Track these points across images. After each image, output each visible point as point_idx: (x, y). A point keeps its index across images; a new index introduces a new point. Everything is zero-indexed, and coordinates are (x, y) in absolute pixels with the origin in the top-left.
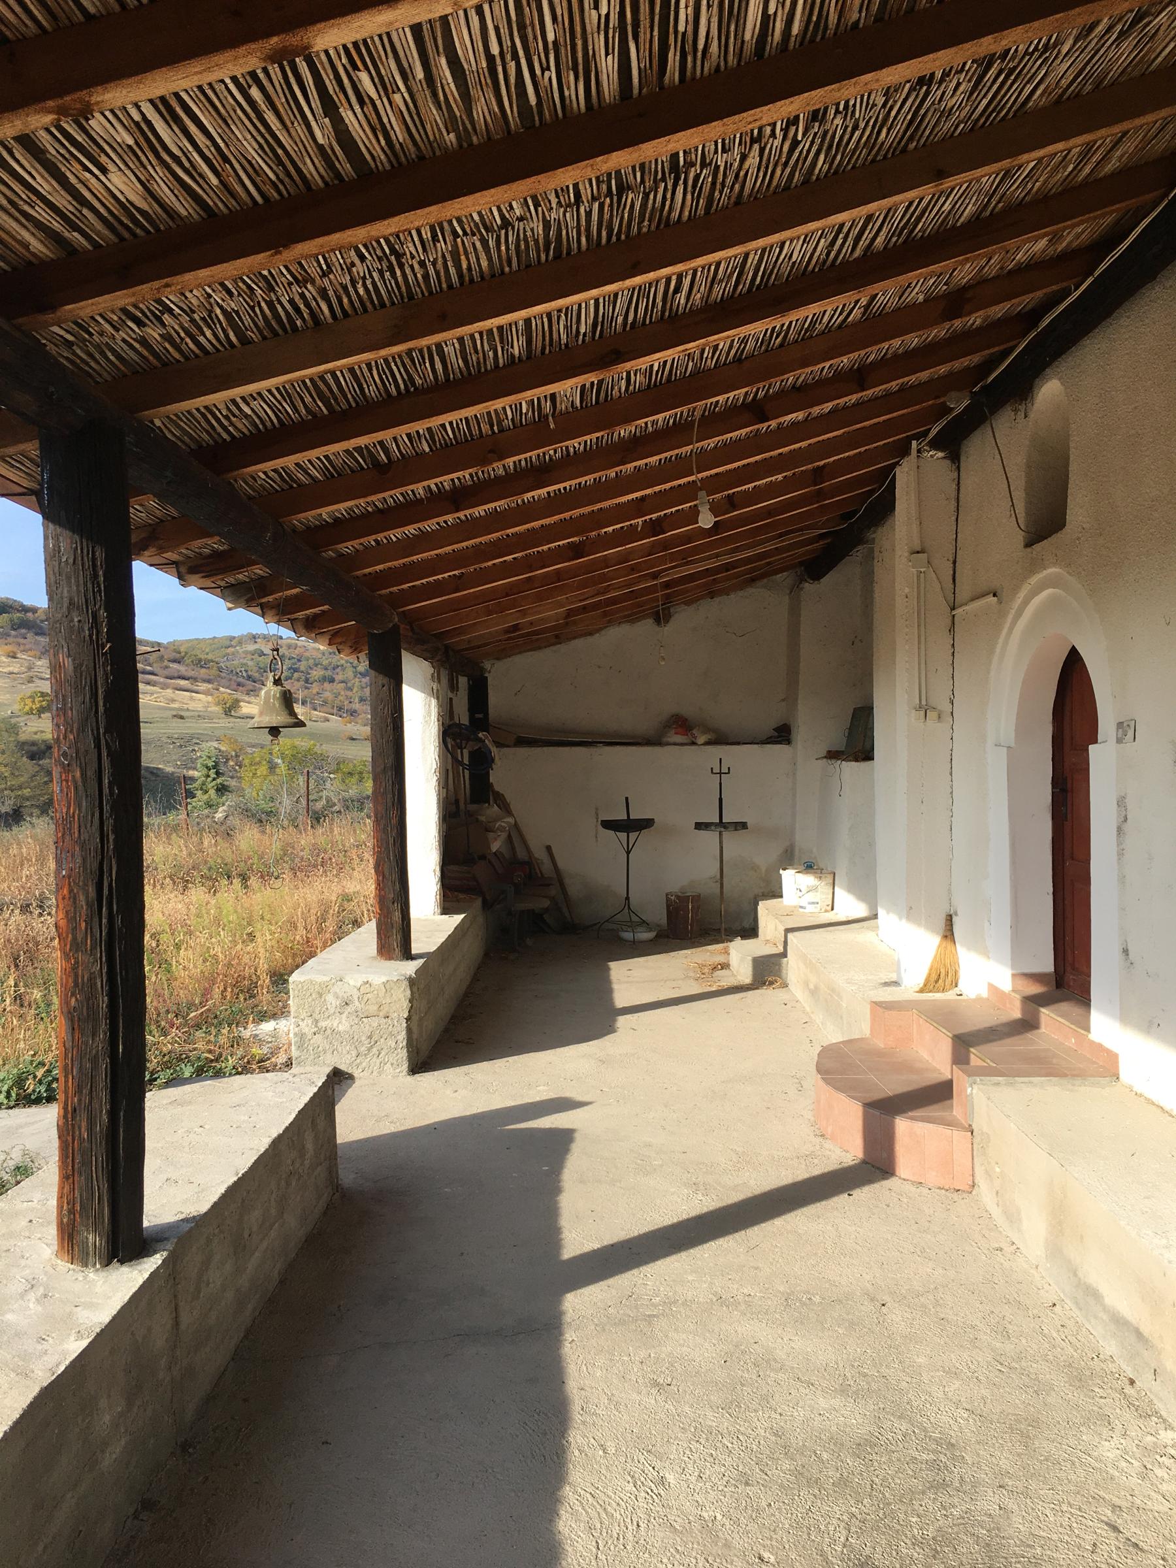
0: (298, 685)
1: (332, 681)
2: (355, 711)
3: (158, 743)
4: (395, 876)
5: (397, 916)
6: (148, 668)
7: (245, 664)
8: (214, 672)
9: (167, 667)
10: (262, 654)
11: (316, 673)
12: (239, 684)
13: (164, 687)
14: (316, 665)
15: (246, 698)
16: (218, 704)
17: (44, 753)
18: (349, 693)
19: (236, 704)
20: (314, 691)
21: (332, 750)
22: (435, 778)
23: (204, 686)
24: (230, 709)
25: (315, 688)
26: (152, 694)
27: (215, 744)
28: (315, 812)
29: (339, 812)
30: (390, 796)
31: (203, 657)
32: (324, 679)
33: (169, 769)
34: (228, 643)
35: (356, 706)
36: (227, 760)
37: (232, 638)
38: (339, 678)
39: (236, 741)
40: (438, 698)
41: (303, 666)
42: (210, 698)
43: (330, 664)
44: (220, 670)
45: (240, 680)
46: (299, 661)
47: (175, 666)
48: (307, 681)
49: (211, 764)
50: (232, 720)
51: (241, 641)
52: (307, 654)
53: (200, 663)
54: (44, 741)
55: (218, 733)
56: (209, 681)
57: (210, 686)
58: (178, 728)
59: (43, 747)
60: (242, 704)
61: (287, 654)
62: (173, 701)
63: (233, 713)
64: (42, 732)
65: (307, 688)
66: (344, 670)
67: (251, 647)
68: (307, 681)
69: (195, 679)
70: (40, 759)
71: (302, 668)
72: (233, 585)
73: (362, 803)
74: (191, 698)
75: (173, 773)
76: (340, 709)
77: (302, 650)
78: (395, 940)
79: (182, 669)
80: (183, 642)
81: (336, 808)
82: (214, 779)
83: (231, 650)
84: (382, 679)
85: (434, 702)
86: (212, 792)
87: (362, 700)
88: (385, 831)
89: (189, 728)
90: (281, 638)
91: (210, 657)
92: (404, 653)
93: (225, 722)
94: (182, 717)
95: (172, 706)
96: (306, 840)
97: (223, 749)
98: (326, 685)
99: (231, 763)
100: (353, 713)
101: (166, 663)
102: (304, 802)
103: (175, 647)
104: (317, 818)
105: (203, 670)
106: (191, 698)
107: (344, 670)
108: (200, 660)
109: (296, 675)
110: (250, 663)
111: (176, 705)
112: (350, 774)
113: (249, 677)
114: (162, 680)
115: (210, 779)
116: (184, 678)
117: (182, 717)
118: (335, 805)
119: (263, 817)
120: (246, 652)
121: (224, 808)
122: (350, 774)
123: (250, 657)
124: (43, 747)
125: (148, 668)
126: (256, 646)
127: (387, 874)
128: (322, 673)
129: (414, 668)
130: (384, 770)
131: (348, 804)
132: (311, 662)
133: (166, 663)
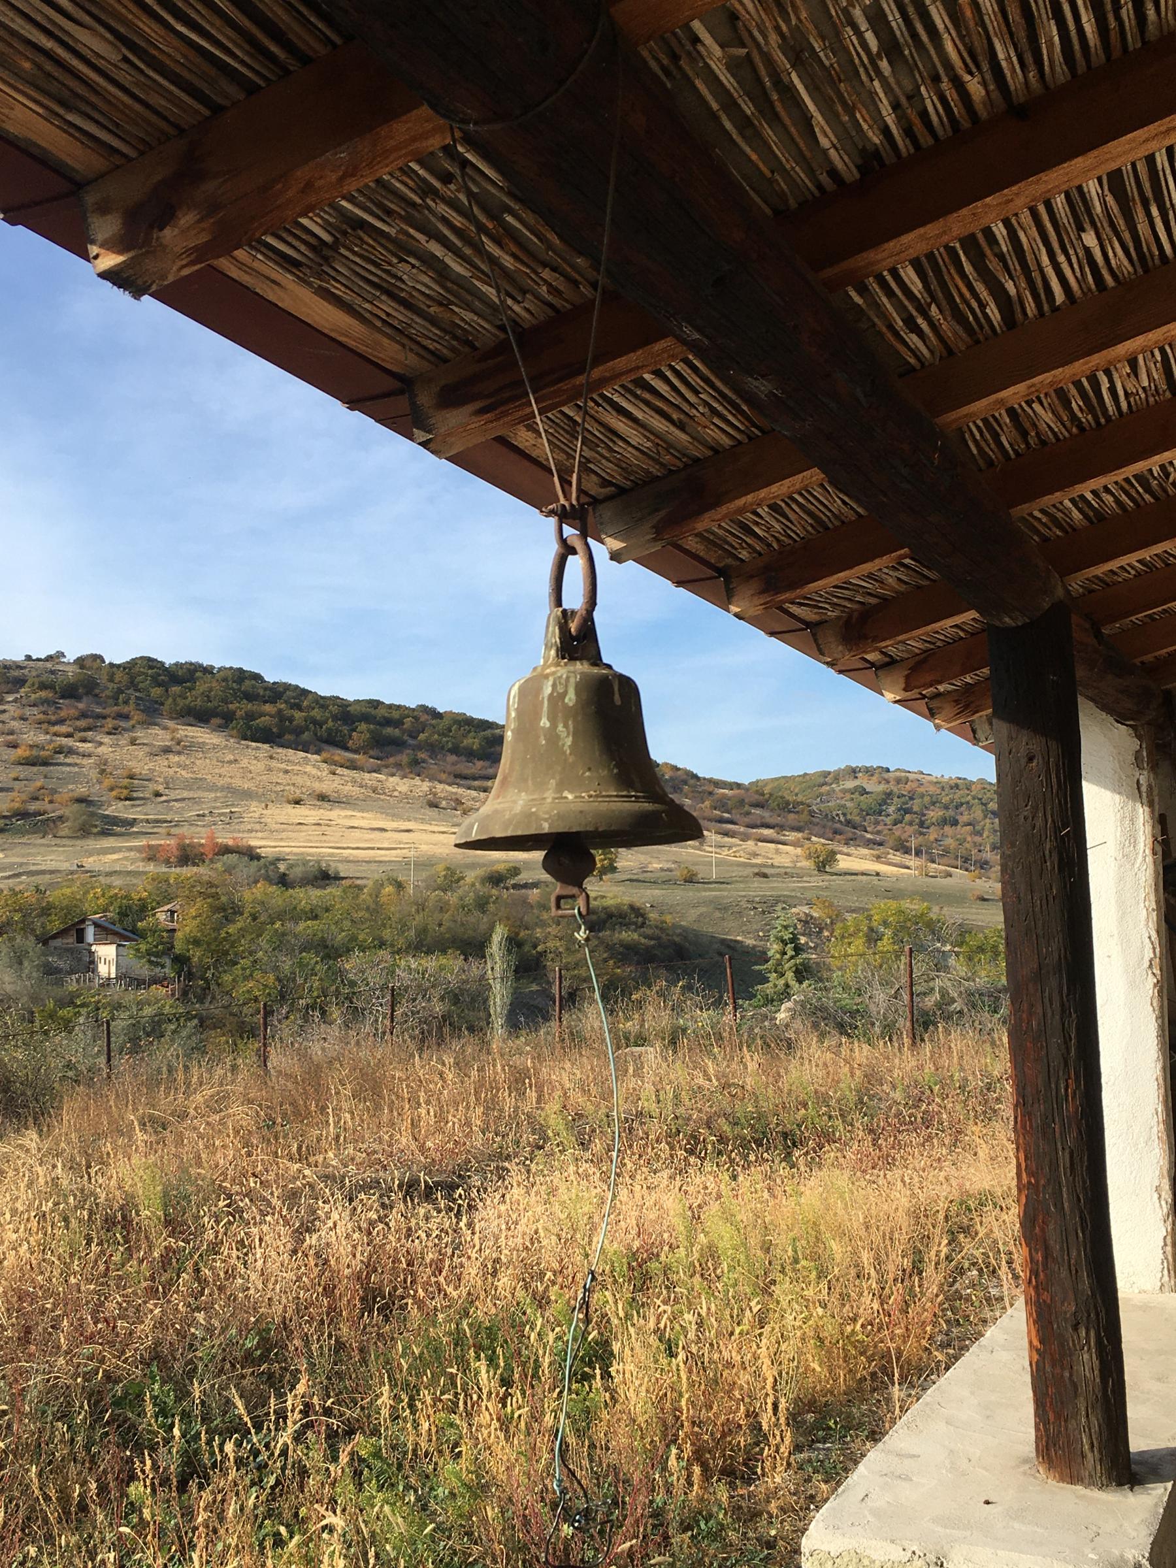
0: (910, 830)
1: (955, 823)
2: (986, 863)
3: (736, 909)
4: (1079, 1255)
5: (1087, 1362)
6: (726, 815)
7: (844, 806)
8: (805, 816)
9: (748, 813)
10: (864, 792)
11: (934, 814)
12: (836, 832)
13: (745, 838)
14: (934, 804)
15: (845, 849)
16: (809, 857)
17: (605, 922)
18: (978, 839)
19: (831, 857)
20: (932, 838)
21: (952, 915)
22: (1152, 980)
23: (793, 836)
24: (824, 863)
25: (933, 834)
26: (730, 848)
27: (806, 909)
28: (925, 1013)
29: (960, 1012)
30: (1056, 1040)
31: (791, 798)
32: (944, 822)
33: (750, 942)
34: (822, 780)
35: (988, 855)
36: (821, 930)
37: (826, 774)
38: (964, 818)
39: (831, 905)
40: (1151, 804)
41: (916, 805)
42: (799, 850)
43: (952, 801)
44: (812, 814)
45: (838, 826)
46: (911, 798)
47: (758, 811)
48: (922, 824)
49: (787, 936)
50: (828, 877)
51: (837, 776)
52: (922, 790)
53: (786, 807)
54: (605, 908)
55: (808, 895)
56: (798, 829)
57: (800, 835)
58: (760, 889)
59: (603, 916)
60: (838, 856)
61: (895, 790)
62: (756, 855)
63: (828, 869)
64: (603, 897)
65: (921, 834)
66: (970, 808)
67: (850, 784)
68: (922, 824)
69: (781, 827)
70: (600, 931)
71: (916, 809)
72: (622, 491)
73: (997, 999)
74: (777, 852)
75: (754, 946)
76: (966, 860)
77: (915, 785)
78: (1085, 1428)
79: (766, 815)
80: (766, 782)
81: (957, 1006)
82: (792, 957)
83: (825, 788)
84: (1027, 742)
85: (1142, 814)
86: (790, 975)
87: (994, 848)
88: (1045, 1131)
89: (773, 888)
90: (888, 770)
91: (800, 798)
92: (1080, 699)
93: (817, 881)
94: (765, 876)
95: (754, 861)
96: (905, 1064)
97: (815, 915)
98: (947, 828)
99: (826, 933)
100: (983, 865)
101: (747, 808)
102: (906, 997)
103: (757, 787)
104: (923, 1024)
105: (791, 816)
106: (777, 852)
107: (970, 808)
108: (788, 803)
109: (908, 817)
110: (849, 804)
111: (758, 861)
112: (981, 949)
113: (848, 823)
114: (742, 829)
115: (786, 957)
116: (768, 826)
117: (765, 876)
118: (953, 1001)
119: (843, 1023)
120: (844, 791)
121: (789, 1004)
122: (981, 949)
123: (848, 796)
124: (603, 916)
125: (726, 815)
126: (857, 783)
127: (1056, 1248)
128: (941, 813)
129: (1104, 744)
130: (1039, 976)
131: (974, 999)
132: (927, 799)
133: (747, 808)
